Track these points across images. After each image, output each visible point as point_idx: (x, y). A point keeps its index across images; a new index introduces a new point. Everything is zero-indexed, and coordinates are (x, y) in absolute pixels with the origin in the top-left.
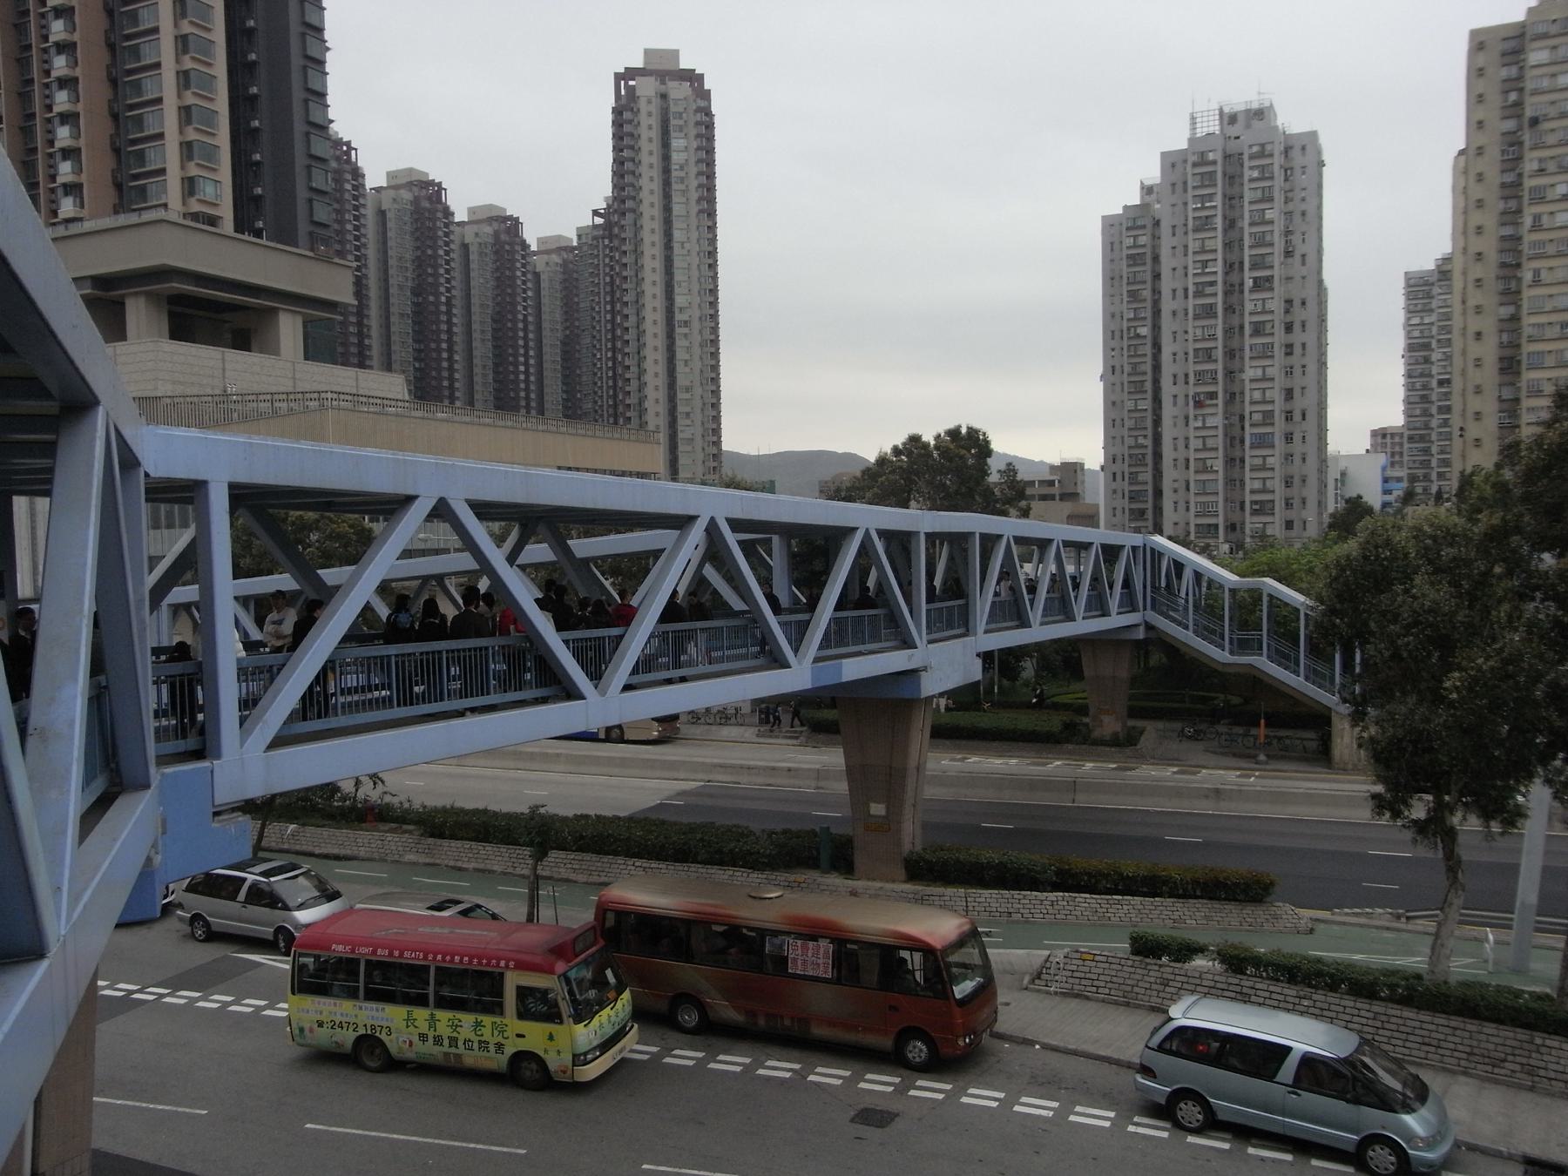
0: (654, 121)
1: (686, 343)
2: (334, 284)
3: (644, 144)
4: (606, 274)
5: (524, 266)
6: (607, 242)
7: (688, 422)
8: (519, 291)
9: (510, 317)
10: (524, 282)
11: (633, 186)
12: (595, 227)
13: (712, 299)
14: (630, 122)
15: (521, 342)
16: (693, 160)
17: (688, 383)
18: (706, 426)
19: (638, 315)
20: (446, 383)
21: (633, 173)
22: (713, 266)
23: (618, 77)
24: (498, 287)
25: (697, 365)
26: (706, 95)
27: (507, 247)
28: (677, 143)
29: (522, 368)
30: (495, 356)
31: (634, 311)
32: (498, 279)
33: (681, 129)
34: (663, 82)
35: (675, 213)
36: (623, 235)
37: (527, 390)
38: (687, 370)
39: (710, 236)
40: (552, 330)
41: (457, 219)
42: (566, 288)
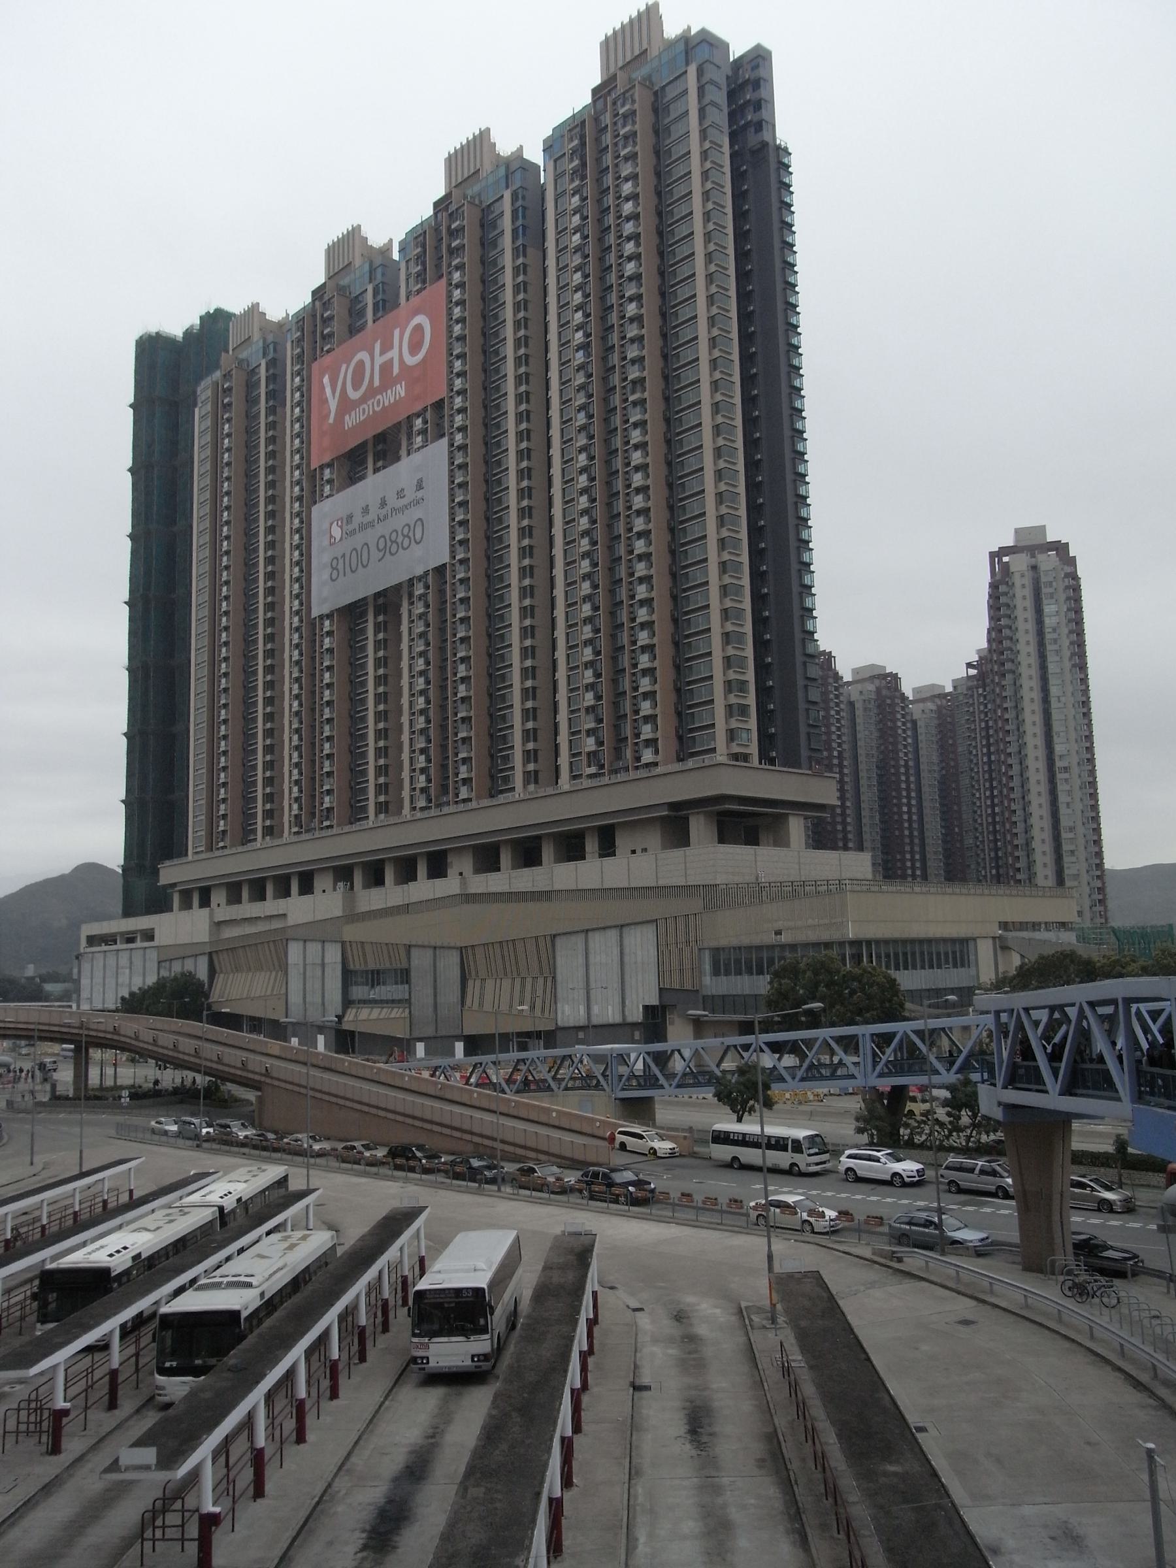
0: (1028, 592)
1: (1067, 787)
2: (825, 791)
3: (1019, 613)
4: (981, 720)
5: (903, 716)
6: (980, 691)
7: (1074, 859)
8: (900, 739)
9: (892, 763)
10: (904, 731)
11: (1011, 649)
12: (969, 677)
13: (1088, 745)
14: (1006, 594)
15: (903, 786)
16: (1064, 621)
17: (1071, 824)
18: (1092, 885)
19: (1022, 775)
20: (839, 827)
21: (1011, 639)
22: (1087, 715)
23: (992, 555)
24: (880, 737)
25: (1078, 806)
26: (1072, 561)
27: (889, 701)
28: (1049, 608)
29: (905, 809)
30: (881, 799)
31: (1018, 761)
32: (880, 730)
33: (1052, 596)
34: (1033, 556)
35: (1050, 671)
36: (1004, 694)
37: (910, 828)
38: (1069, 811)
39: (1083, 687)
40: (930, 771)
41: (845, 680)
42: (940, 732)
